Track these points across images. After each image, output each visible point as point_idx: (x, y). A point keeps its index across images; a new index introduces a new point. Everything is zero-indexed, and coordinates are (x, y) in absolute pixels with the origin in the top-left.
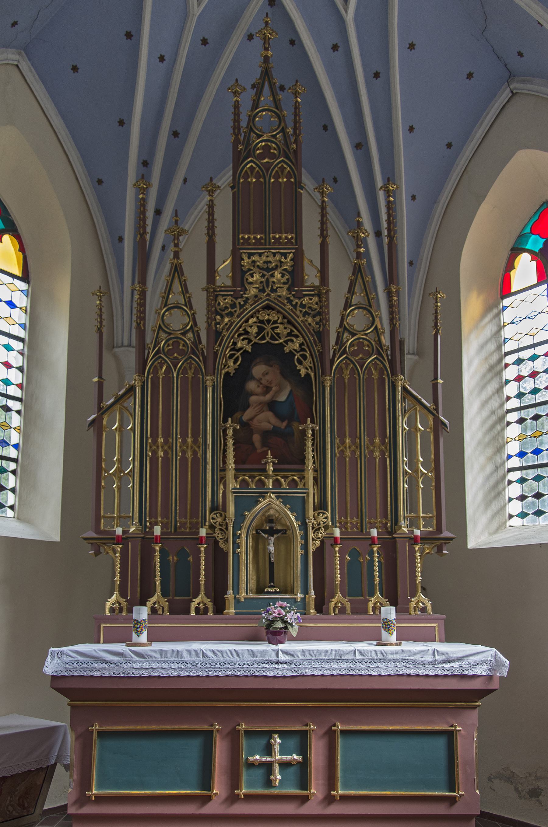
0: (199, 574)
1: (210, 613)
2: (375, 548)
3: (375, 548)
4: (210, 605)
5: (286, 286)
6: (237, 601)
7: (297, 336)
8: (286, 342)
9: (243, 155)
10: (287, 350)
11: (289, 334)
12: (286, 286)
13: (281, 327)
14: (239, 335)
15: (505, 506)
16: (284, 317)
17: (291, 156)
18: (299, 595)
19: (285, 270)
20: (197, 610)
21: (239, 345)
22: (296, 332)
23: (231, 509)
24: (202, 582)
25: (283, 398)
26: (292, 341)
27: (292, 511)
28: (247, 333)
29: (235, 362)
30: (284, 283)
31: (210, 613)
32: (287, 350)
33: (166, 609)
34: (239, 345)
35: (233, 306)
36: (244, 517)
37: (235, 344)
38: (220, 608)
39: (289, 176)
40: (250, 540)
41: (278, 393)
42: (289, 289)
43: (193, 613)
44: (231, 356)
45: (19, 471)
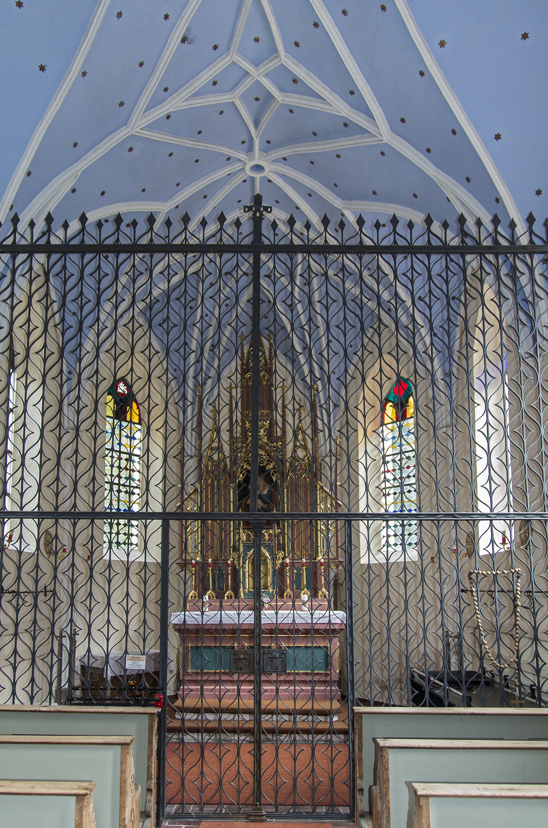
0: (228, 581)
1: (233, 598)
2: (304, 568)
3: (304, 568)
4: (233, 595)
5: (266, 437)
6: (244, 592)
7: (271, 462)
8: (267, 464)
9: (246, 371)
10: (267, 469)
11: (268, 461)
12: (266, 437)
13: (264, 457)
14: (245, 462)
15: (381, 540)
16: (266, 452)
17: (268, 371)
18: (271, 590)
19: (266, 429)
20: (228, 597)
21: (245, 467)
22: (271, 460)
23: (241, 550)
24: (230, 584)
25: (265, 492)
26: (269, 464)
27: (267, 551)
28: (248, 461)
29: (243, 475)
30: (266, 436)
31: (233, 598)
32: (267, 469)
33: (214, 596)
34: (245, 467)
35: (242, 447)
36: (247, 554)
37: (243, 466)
38: (237, 595)
39: (267, 381)
40: (250, 565)
41: (263, 491)
42: (268, 438)
43: (226, 598)
44: (241, 472)
45: (139, 525)
